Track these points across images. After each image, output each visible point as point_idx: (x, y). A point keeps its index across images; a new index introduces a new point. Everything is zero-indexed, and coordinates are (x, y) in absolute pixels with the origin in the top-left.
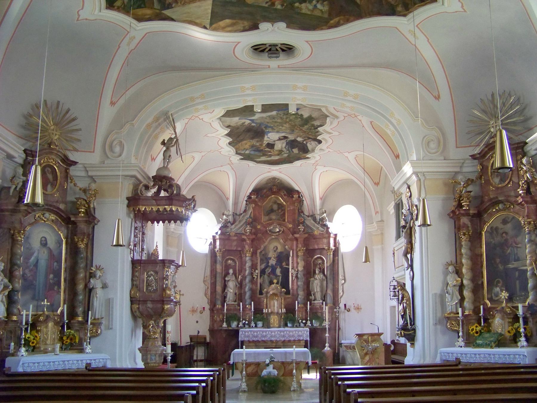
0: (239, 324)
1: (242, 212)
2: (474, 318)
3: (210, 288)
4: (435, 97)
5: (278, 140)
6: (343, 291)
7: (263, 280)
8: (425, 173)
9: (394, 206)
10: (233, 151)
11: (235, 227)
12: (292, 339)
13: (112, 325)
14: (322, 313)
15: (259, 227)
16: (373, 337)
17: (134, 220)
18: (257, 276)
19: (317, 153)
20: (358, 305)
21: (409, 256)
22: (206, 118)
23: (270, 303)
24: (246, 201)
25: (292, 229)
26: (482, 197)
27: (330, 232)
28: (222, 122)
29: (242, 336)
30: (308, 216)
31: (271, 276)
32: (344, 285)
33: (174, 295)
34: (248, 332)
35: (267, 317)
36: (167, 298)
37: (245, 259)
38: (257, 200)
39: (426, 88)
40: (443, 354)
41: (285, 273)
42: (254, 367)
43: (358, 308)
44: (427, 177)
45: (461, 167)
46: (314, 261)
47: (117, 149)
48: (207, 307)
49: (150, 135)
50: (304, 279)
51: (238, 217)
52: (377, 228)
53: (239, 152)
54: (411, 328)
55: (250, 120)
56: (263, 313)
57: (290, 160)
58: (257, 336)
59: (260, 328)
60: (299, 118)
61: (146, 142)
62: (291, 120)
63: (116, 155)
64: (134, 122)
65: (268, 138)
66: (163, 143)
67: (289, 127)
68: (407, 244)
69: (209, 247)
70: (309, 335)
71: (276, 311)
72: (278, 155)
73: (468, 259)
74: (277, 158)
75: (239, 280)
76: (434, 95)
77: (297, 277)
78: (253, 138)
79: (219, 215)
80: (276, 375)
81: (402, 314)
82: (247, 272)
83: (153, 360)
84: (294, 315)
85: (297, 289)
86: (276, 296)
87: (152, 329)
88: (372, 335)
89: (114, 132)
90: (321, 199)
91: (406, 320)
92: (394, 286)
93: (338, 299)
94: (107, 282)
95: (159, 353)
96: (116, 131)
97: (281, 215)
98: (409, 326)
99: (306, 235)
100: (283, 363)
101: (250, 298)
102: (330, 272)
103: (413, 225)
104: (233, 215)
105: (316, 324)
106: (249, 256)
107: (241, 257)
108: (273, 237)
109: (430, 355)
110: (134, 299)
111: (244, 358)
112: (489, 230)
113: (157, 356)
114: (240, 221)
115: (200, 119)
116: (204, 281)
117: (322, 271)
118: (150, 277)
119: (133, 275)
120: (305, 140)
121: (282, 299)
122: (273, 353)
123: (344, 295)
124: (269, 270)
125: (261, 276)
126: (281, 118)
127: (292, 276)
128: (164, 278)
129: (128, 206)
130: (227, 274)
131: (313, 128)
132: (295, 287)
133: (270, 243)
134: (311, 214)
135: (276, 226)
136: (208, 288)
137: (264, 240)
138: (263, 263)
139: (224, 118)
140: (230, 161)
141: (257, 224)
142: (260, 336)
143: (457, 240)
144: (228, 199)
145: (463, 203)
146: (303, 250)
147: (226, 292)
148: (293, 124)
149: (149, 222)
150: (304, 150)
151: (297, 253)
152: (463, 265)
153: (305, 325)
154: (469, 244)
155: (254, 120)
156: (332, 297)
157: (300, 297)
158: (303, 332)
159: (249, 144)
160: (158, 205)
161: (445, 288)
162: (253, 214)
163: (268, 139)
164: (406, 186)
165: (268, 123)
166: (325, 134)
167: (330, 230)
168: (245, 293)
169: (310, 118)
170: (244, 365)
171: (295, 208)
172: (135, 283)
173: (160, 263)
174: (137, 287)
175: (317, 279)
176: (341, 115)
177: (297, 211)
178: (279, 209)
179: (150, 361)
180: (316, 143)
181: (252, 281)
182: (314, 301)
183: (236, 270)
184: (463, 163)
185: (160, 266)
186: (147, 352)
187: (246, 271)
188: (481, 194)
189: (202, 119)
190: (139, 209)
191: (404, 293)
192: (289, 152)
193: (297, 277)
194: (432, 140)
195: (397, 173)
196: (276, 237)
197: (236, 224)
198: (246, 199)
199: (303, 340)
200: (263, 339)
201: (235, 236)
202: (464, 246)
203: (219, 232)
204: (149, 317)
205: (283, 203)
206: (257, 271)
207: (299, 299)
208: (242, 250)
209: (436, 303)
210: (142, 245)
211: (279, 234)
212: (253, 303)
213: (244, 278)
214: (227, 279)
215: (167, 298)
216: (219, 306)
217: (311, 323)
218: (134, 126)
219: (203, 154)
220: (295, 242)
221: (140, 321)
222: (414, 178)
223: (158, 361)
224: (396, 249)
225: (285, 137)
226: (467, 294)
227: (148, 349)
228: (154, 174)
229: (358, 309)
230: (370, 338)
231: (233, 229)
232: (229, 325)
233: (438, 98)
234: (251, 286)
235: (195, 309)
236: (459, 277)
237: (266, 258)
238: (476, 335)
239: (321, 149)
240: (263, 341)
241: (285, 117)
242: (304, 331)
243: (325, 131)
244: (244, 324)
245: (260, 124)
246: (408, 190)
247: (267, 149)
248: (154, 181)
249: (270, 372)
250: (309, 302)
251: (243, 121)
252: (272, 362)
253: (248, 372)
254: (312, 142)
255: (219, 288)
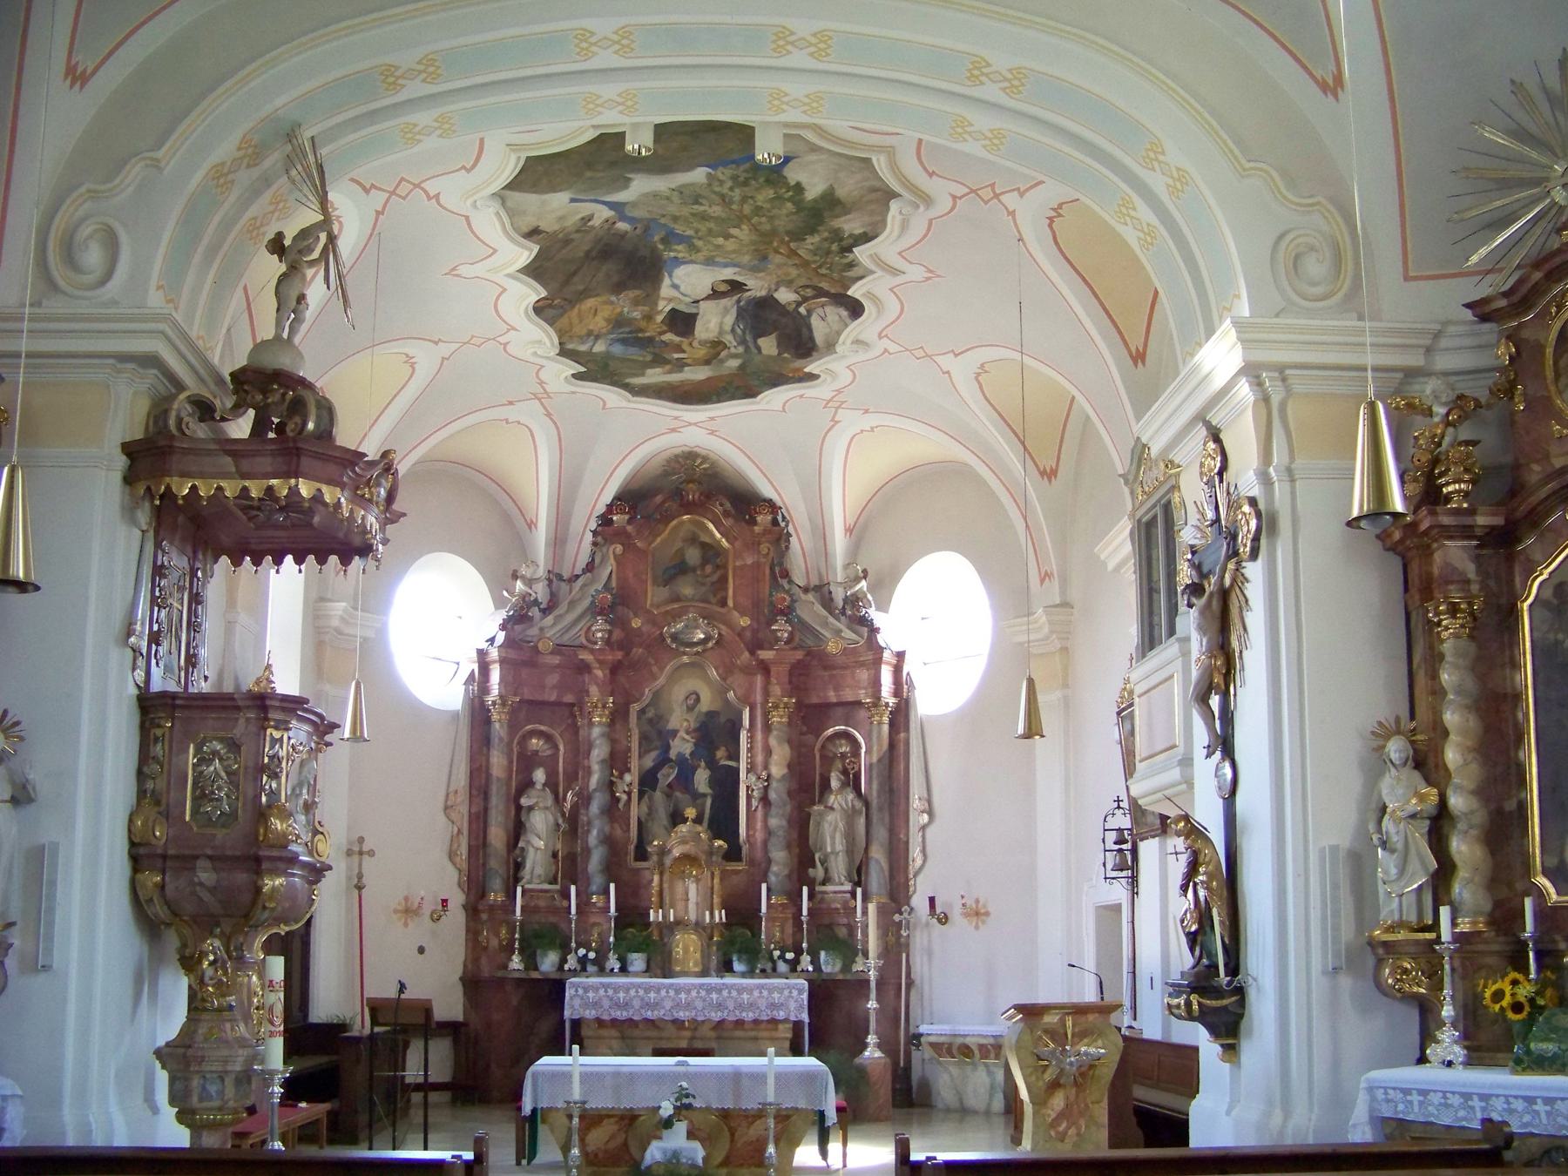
0: (566, 961)
1: (578, 571)
2: (1495, 947)
3: (465, 832)
4: (1324, 87)
5: (708, 298)
6: (924, 851)
7: (650, 808)
8: (1288, 372)
9: (1132, 533)
10: (551, 339)
11: (554, 624)
12: (748, 1016)
13: (49, 951)
14: (851, 929)
15: (636, 623)
16: (1082, 1019)
17: (151, 534)
18: (629, 794)
19: (844, 357)
20: (977, 901)
21: (1215, 701)
22: (454, 190)
23: (672, 888)
24: (595, 533)
25: (748, 634)
26: (1516, 467)
27: (883, 645)
28: (512, 213)
29: (577, 1002)
30: (806, 590)
31: (678, 794)
32: (929, 831)
33: (306, 837)
34: (596, 989)
35: (662, 938)
36: (272, 846)
37: (589, 734)
38: (629, 528)
39: (987, 465)
40: (1380, 1094)
41: (726, 783)
42: (616, 1127)
43: (977, 914)
44: (1298, 388)
45: (1429, 350)
46: (823, 747)
47: (93, 257)
48: (457, 899)
49: (227, 226)
50: (788, 808)
51: (564, 587)
52: (1046, 630)
53: (570, 346)
54: (1229, 983)
55: (611, 205)
56: (648, 924)
57: (743, 386)
58: (626, 1005)
59: (636, 974)
60: (789, 200)
61: (213, 250)
62: (758, 210)
63: (88, 279)
64: (159, 154)
65: (675, 287)
66: (277, 246)
67: (753, 243)
68: (1211, 655)
69: (467, 690)
70: (806, 1002)
71: (692, 916)
72: (707, 362)
73: (1467, 707)
74: (698, 374)
75: (568, 805)
76: (1318, 73)
77: (765, 799)
78: (618, 288)
79: (499, 577)
80: (700, 1162)
81: (1194, 928)
82: (594, 780)
83: (210, 1098)
84: (756, 933)
85: (765, 843)
86: (691, 866)
87: (209, 972)
88: (1079, 1010)
89: (83, 189)
90: (849, 530)
91: (1208, 952)
92: (1120, 830)
93: (907, 880)
94: (31, 777)
95: (238, 1068)
96: (92, 186)
97: (713, 584)
98: (1223, 978)
99: (799, 655)
100: (725, 1114)
101: (602, 871)
102: (881, 785)
103: (1234, 580)
104: (550, 581)
105: (830, 965)
106: (600, 723)
107: (575, 729)
108: (685, 659)
109: (1310, 1090)
110: (142, 851)
111: (577, 1094)
112: (1548, 593)
113: (229, 1081)
114: (572, 604)
115: (429, 198)
116: (446, 808)
117: (852, 781)
118: (209, 762)
119: (144, 756)
120: (805, 299)
121: (713, 874)
122: (686, 1076)
123: (927, 865)
124: (668, 775)
125: (641, 794)
126: (723, 197)
127: (749, 797)
128: (262, 769)
129: (129, 479)
130: (526, 785)
131: (834, 247)
132: (759, 836)
133: (672, 679)
134: (815, 581)
135: (695, 620)
136: (459, 831)
137: (655, 669)
138: (648, 751)
139: (516, 197)
140: (541, 383)
141: (631, 615)
142: (636, 1003)
143: (1418, 633)
144: (531, 525)
145: (1448, 484)
146: (786, 706)
147: (523, 849)
148: (767, 227)
149: (225, 560)
150: (801, 344)
151: (766, 715)
152: (1446, 733)
153: (793, 970)
154: (1472, 648)
155: (624, 204)
156: (887, 874)
157: (774, 868)
158: (786, 992)
159: (606, 312)
160: (244, 476)
161: (1372, 827)
162: (618, 578)
163: (675, 293)
164: (1204, 432)
165: (675, 219)
166: (879, 273)
167: (882, 639)
168: (587, 851)
169: (830, 203)
170: (576, 1121)
171: (763, 560)
172: (150, 785)
173: (248, 707)
174: (158, 803)
175: (832, 808)
176: (940, 190)
177: (767, 571)
178: (705, 561)
179: (201, 1100)
180: (844, 313)
181: (613, 810)
182: (823, 883)
183: (557, 773)
184: (1437, 335)
185: (248, 719)
186: (188, 1065)
187: (589, 772)
188: (1508, 459)
189: (437, 196)
190: (168, 488)
191: (1199, 844)
192: (747, 349)
193: (765, 799)
194: (1312, 248)
195: (1138, 421)
196: (694, 659)
197: (557, 612)
198: (593, 525)
199: (786, 1020)
200: (649, 1015)
201: (552, 653)
202: (1448, 658)
203: (501, 637)
204: (205, 923)
205: (719, 542)
206: (628, 778)
207: (772, 878)
208: (580, 704)
209: (1335, 887)
210: (188, 644)
211: (704, 651)
212: (612, 886)
213: (584, 799)
214: (524, 801)
215: (272, 846)
216: (496, 896)
217: (812, 963)
218: (160, 169)
219: (445, 350)
220: (759, 680)
221: (172, 940)
222: (1244, 390)
223: (231, 1104)
224: (1138, 690)
225: (736, 287)
226: (1464, 848)
227: (190, 1052)
228: (241, 361)
229: (977, 914)
230: (1069, 1023)
231: (549, 630)
232: (531, 962)
233: (1332, 87)
234: (607, 829)
235: (416, 905)
236: (1429, 782)
237: (660, 733)
238: (1511, 1015)
239: (857, 342)
240: (647, 1020)
241: (737, 194)
242: (789, 987)
243: (876, 259)
244: (583, 961)
245: (648, 226)
246: (1211, 445)
247: (669, 337)
248: (236, 392)
249: (676, 1154)
250: (805, 889)
251: (586, 208)
252: (683, 1109)
253: (590, 1149)
254: (828, 309)
255: (497, 835)
